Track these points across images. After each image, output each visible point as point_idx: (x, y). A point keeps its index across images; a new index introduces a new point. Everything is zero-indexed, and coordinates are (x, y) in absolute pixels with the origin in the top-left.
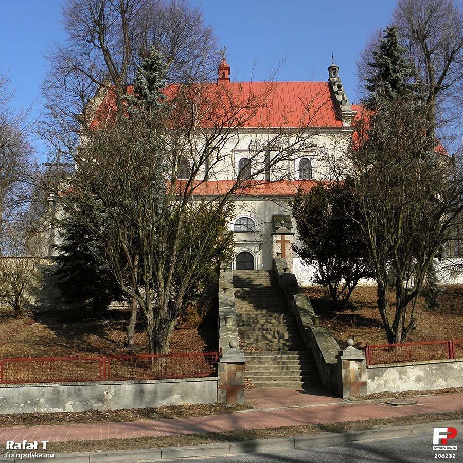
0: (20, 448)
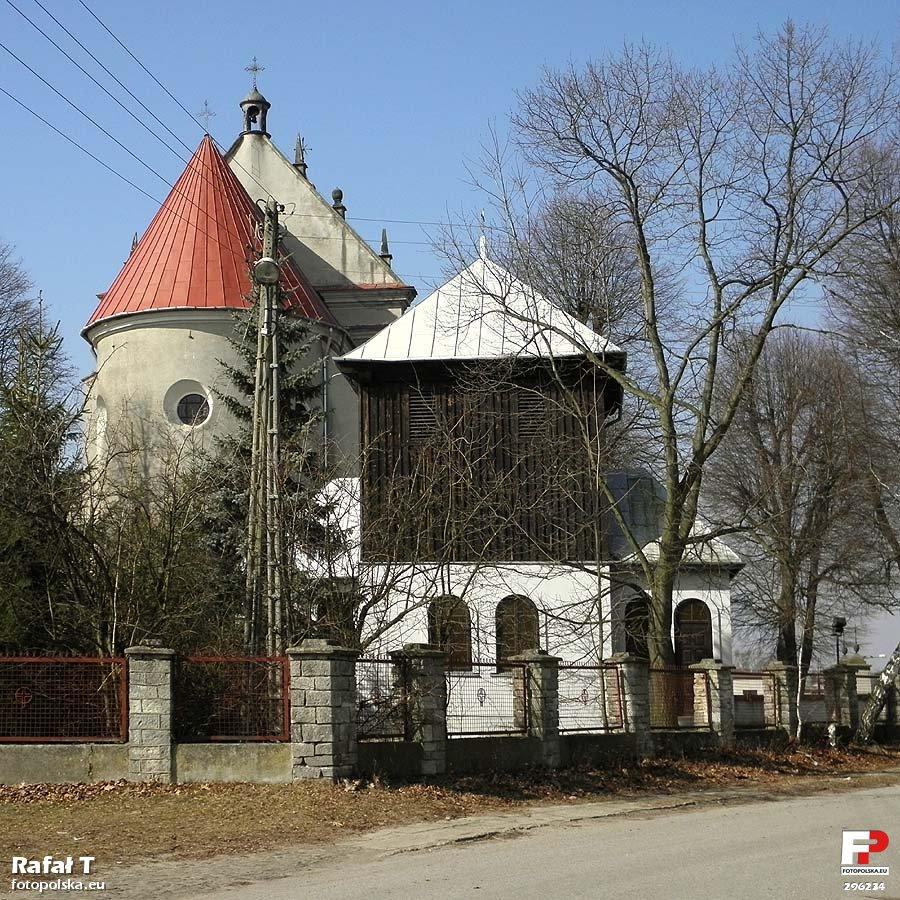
0: (38, 871)
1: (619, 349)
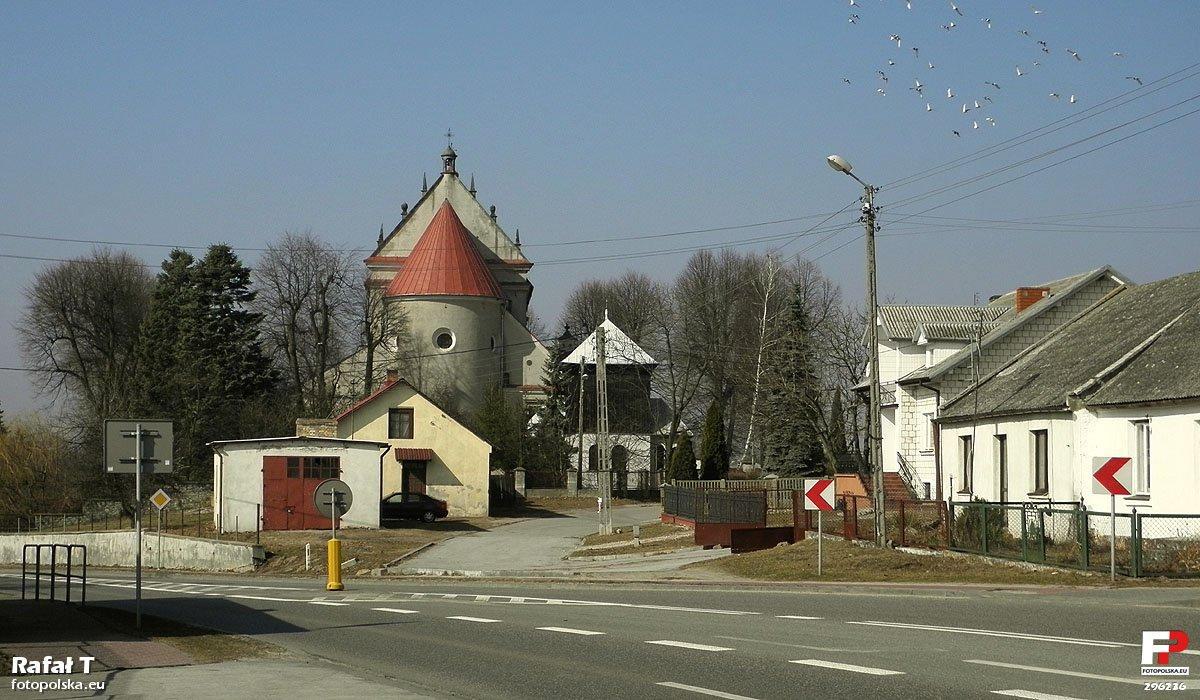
0: (38, 671)
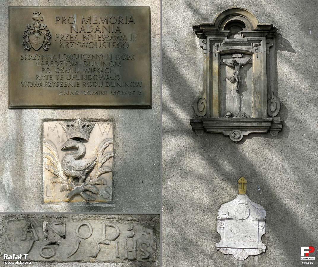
0: (11, 258)
1: (279, 125)
